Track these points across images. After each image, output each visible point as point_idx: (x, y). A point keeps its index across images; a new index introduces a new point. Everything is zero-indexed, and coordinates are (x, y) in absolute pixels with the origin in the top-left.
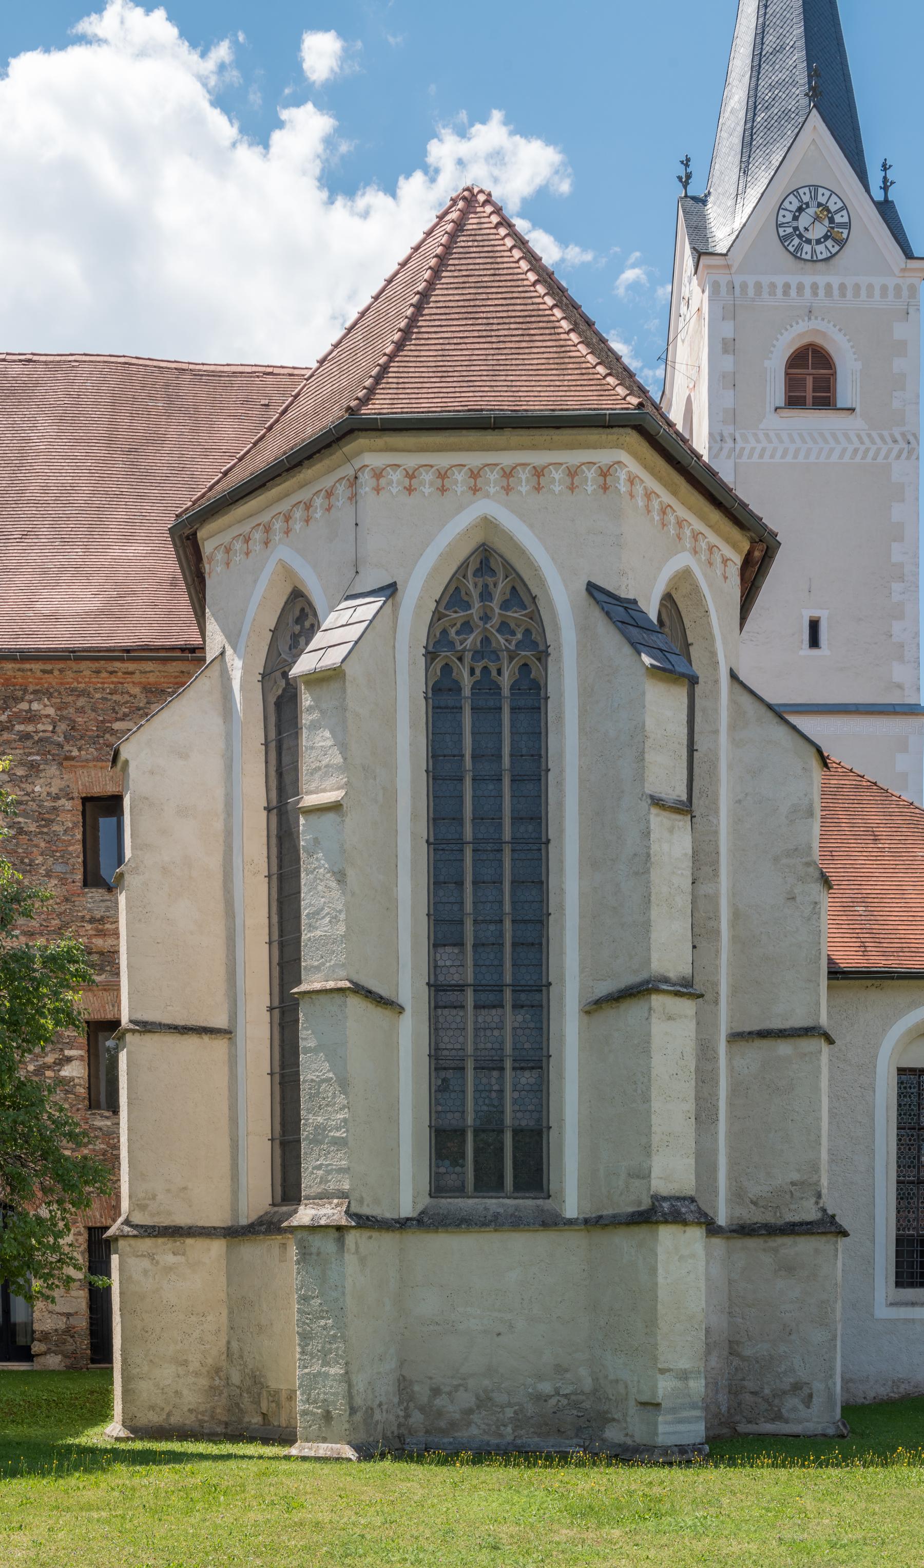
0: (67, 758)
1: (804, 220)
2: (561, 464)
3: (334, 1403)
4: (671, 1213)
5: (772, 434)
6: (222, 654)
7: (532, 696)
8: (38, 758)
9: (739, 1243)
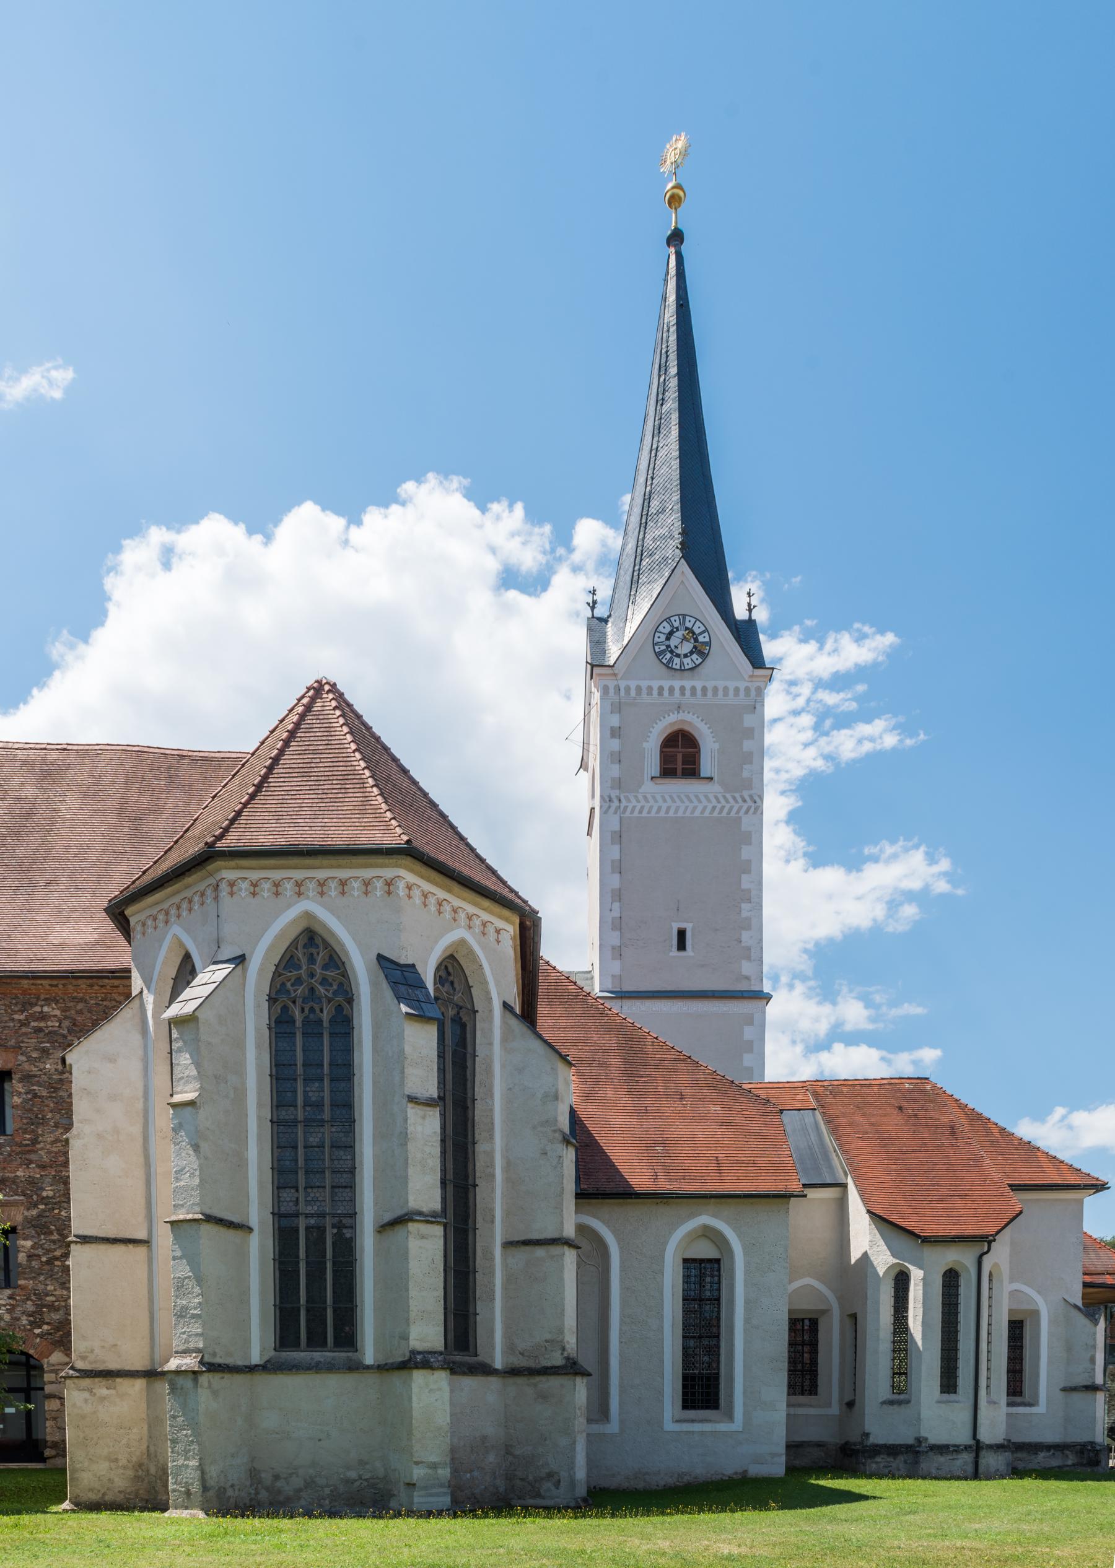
1: (674, 642)
3: (192, 1484)
4: (422, 1362)
5: (648, 796)
6: (141, 992)
7: (343, 1025)
9: (511, 1380)
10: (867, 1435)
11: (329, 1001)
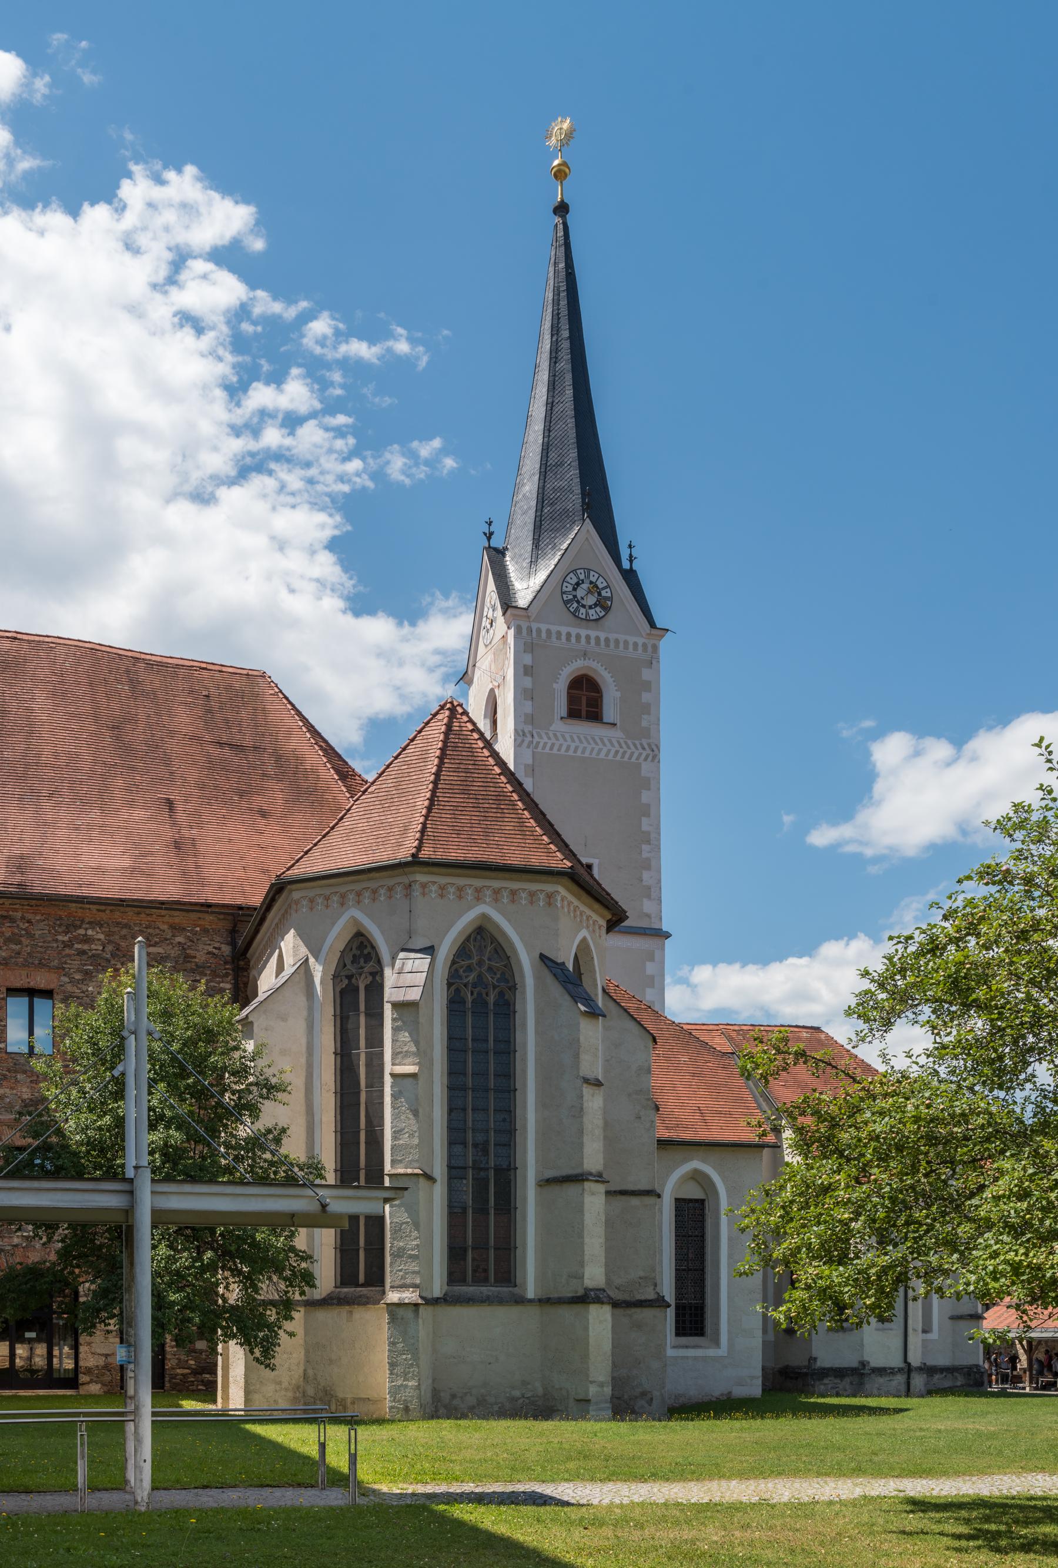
1: (580, 593)
3: (411, 1402)
5: (558, 734)
10: (815, 1359)
11: (495, 987)
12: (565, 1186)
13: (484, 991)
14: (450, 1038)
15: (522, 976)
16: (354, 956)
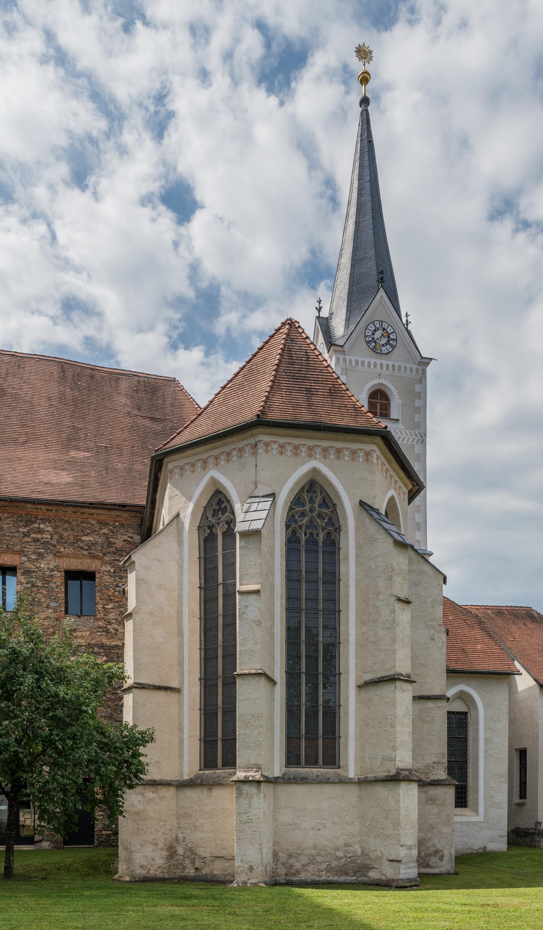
0: (58, 552)
1: (378, 334)
2: (349, 448)
7: (332, 546)
8: (43, 551)
10: (540, 823)
12: (380, 685)
13: (315, 532)
14: (288, 570)
15: (345, 518)
16: (214, 511)
